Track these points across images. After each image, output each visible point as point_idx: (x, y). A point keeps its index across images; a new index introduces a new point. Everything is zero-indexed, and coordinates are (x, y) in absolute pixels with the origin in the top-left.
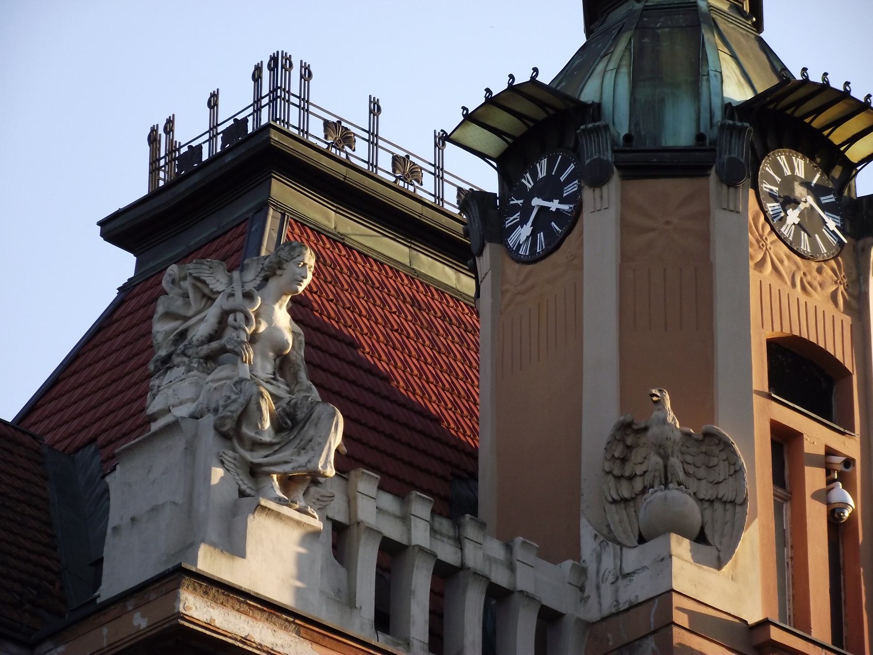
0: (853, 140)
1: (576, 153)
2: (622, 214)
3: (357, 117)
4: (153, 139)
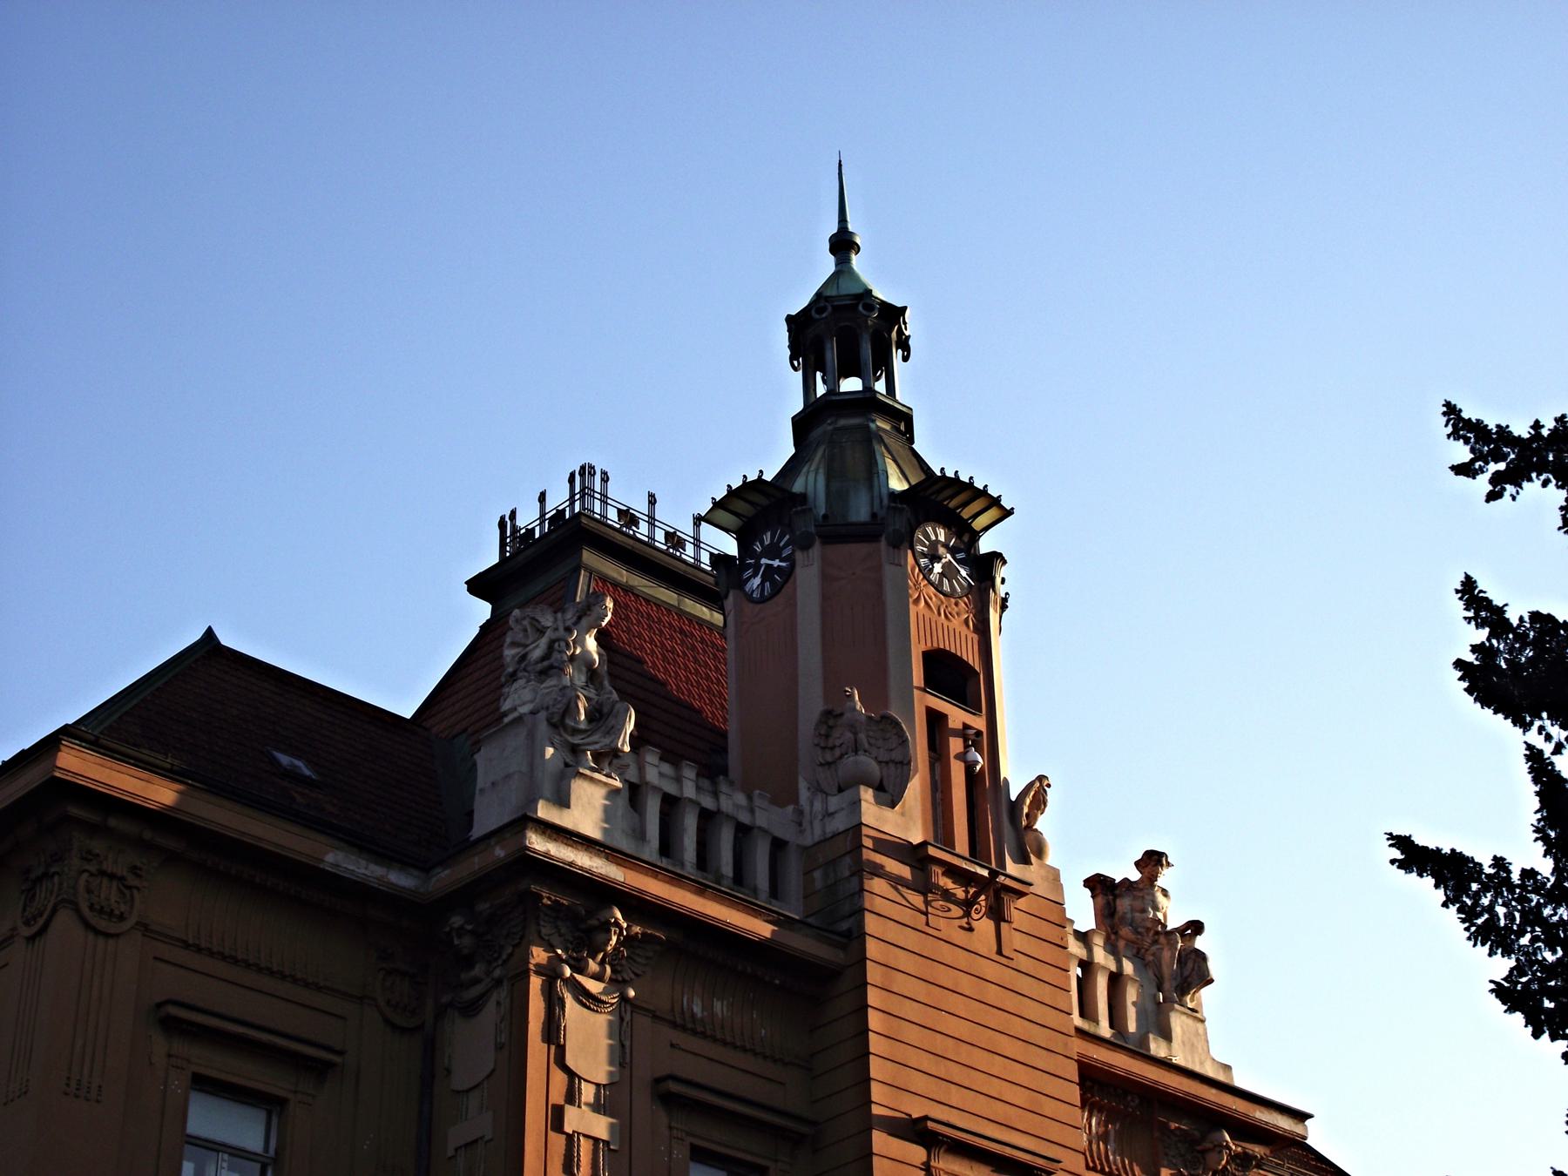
3: (640, 506)
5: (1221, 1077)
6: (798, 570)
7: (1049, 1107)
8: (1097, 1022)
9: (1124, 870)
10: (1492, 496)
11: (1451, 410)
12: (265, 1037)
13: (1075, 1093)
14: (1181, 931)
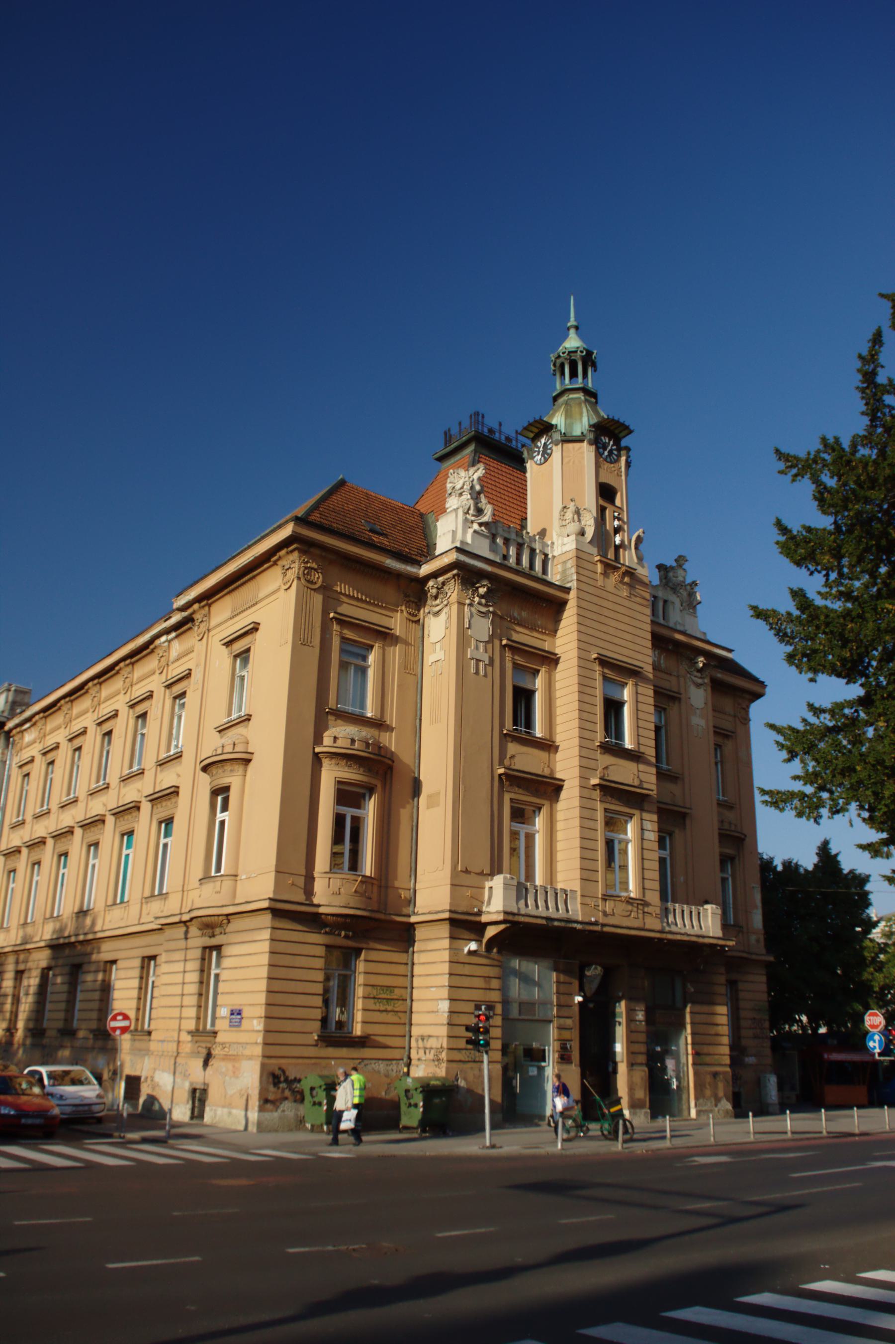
0: (620, 432)
1: (551, 437)
2: (604, 689)
3: (495, 426)
4: (445, 433)
5: (702, 637)
6: (554, 454)
7: (639, 641)
8: (658, 617)
9: (670, 562)
10: (793, 481)
11: (777, 451)
12: (367, 624)
13: (649, 644)
14: (690, 585)
